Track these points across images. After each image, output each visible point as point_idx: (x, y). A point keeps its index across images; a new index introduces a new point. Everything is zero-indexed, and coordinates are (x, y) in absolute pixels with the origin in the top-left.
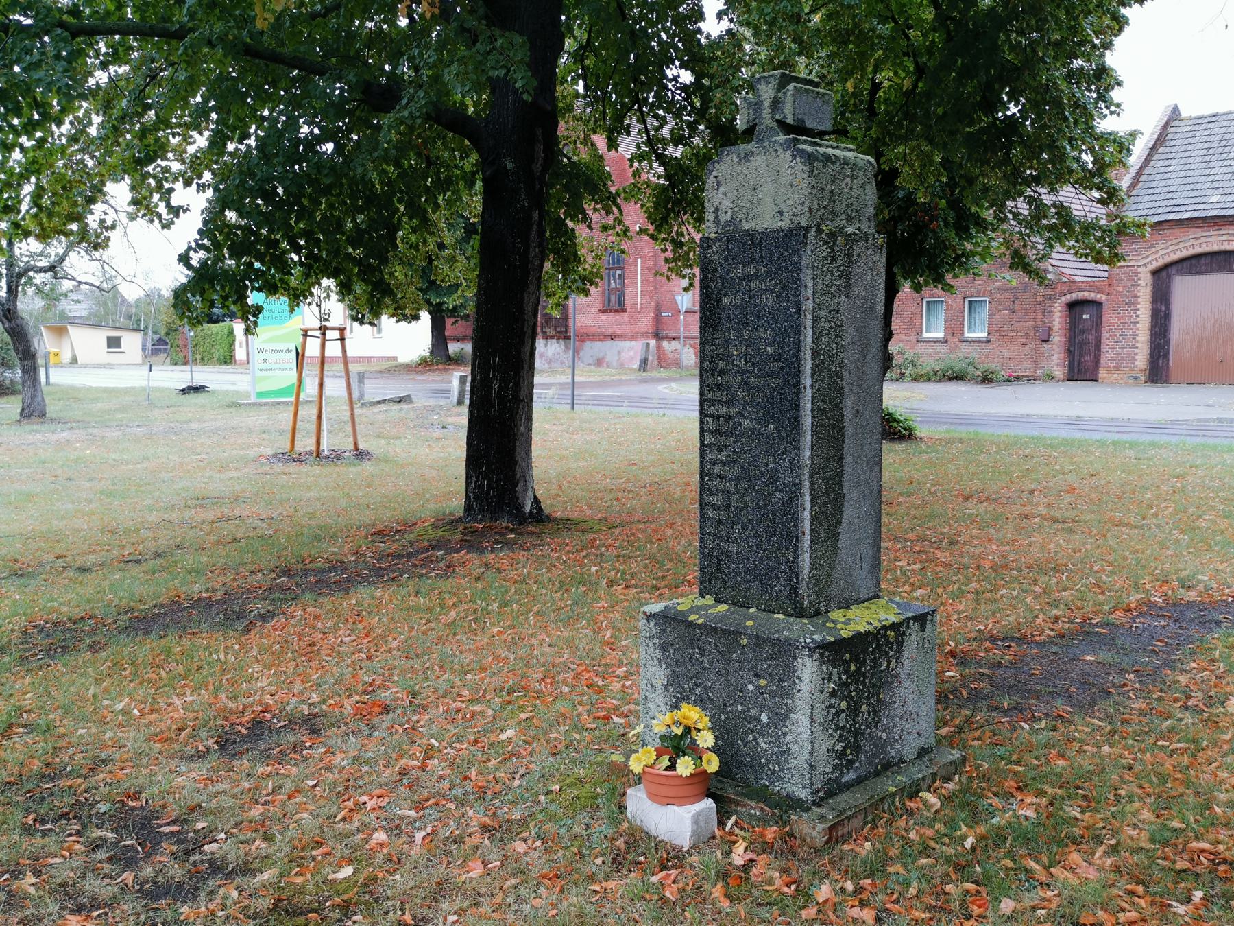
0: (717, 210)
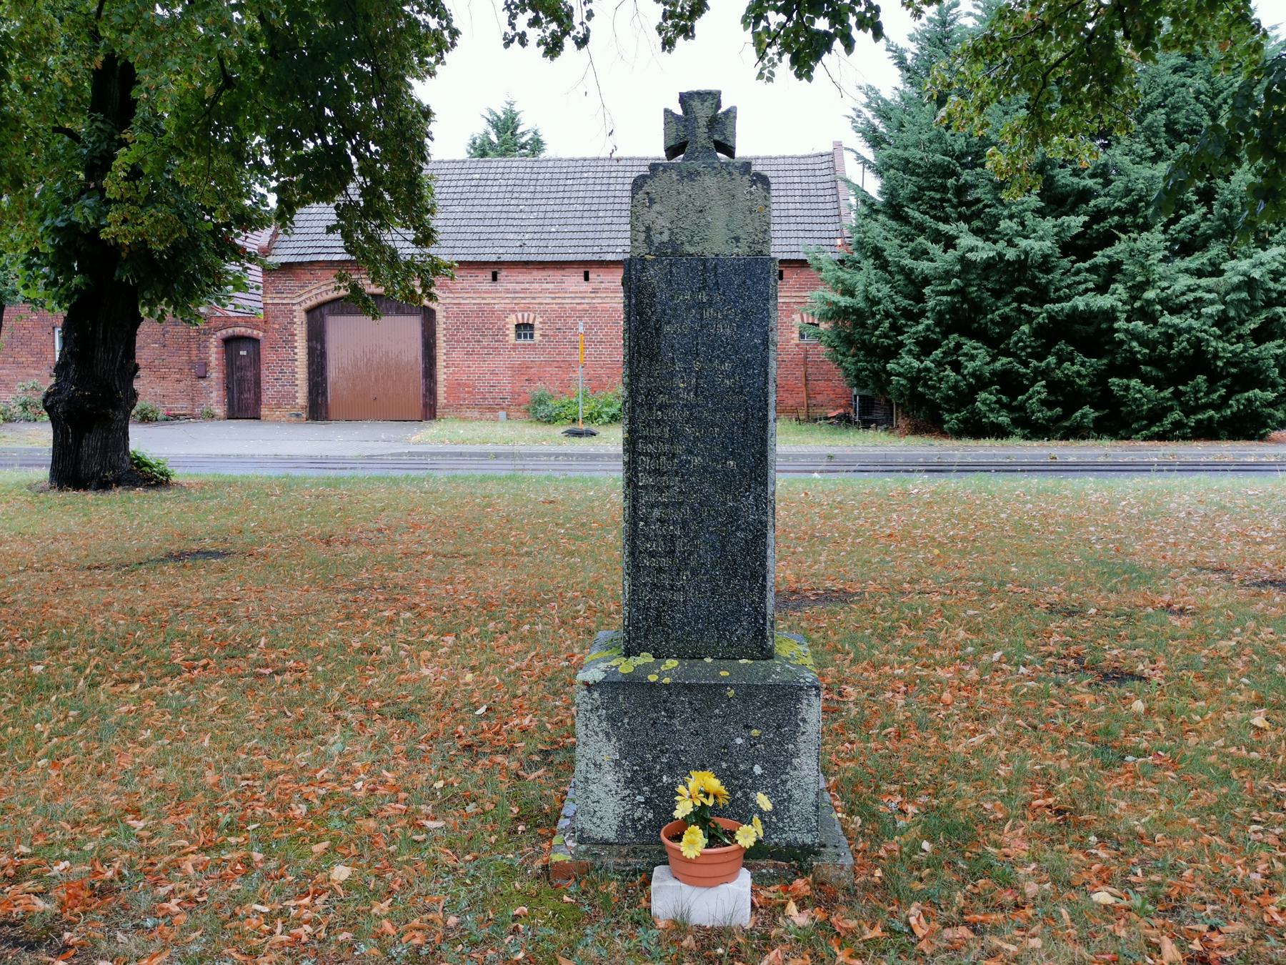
0: (648, 229)
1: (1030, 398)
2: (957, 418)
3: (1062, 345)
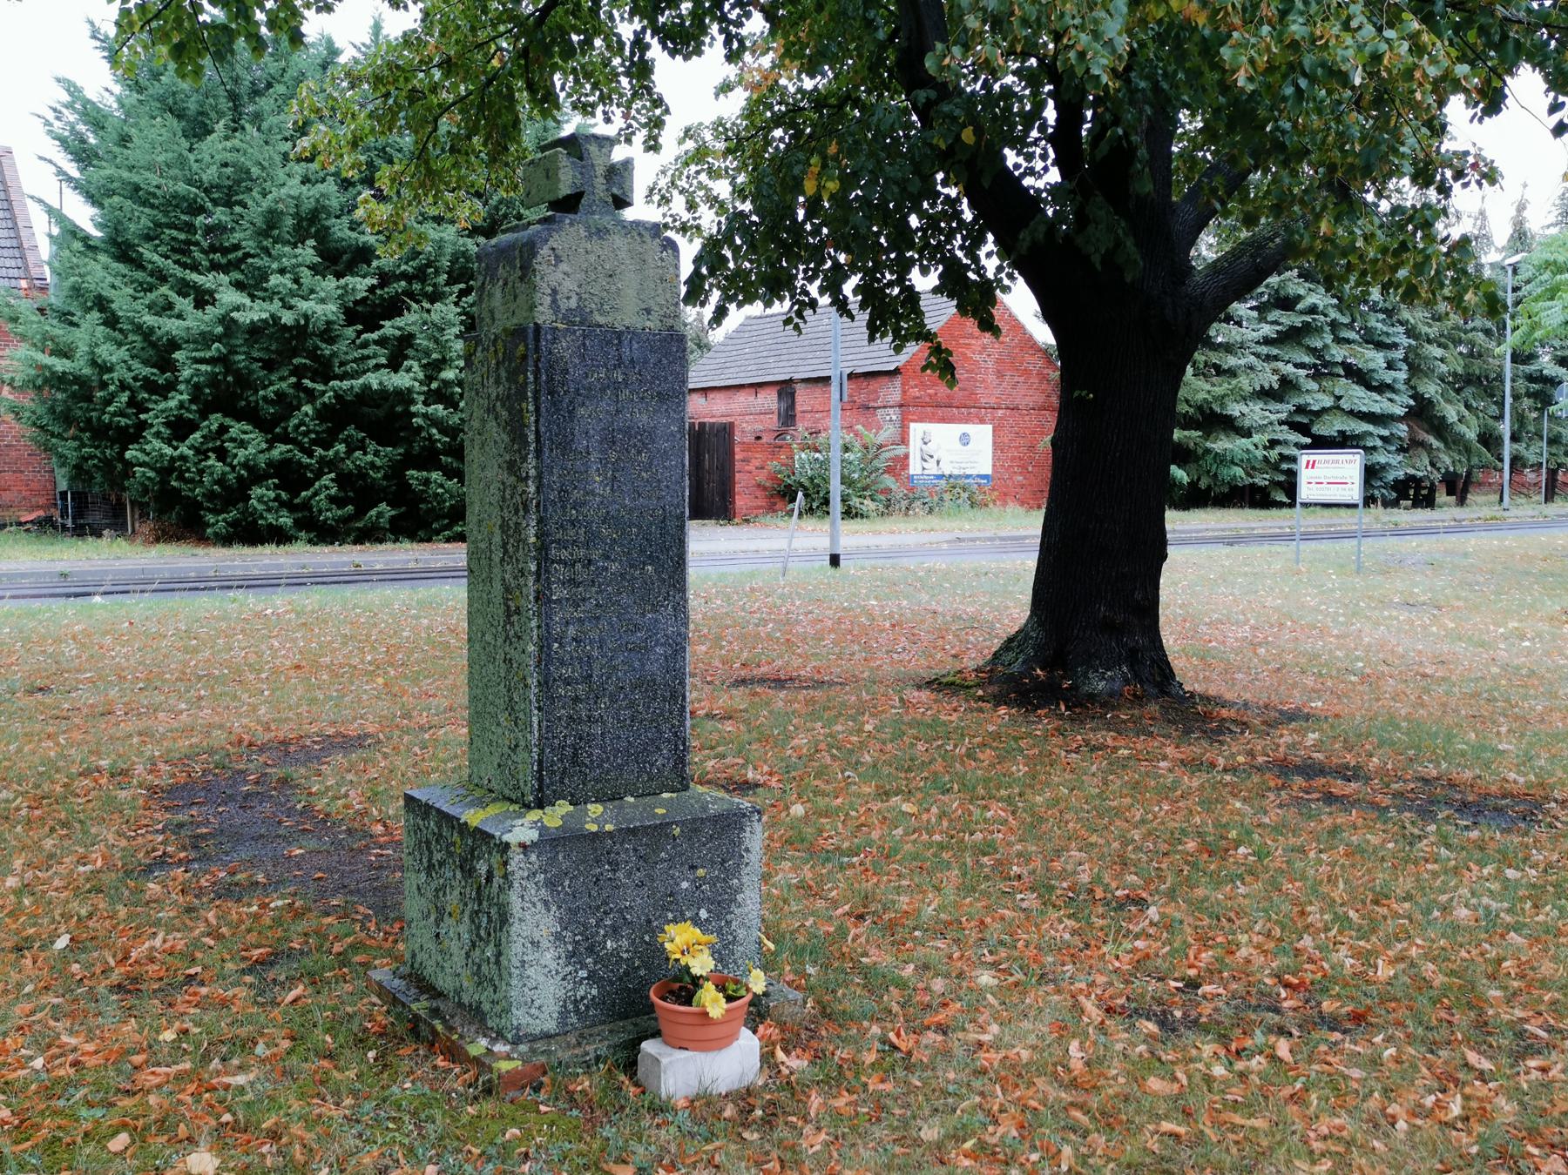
0: (554, 292)
1: (316, 494)
2: (224, 520)
3: (351, 430)
